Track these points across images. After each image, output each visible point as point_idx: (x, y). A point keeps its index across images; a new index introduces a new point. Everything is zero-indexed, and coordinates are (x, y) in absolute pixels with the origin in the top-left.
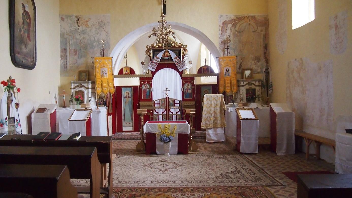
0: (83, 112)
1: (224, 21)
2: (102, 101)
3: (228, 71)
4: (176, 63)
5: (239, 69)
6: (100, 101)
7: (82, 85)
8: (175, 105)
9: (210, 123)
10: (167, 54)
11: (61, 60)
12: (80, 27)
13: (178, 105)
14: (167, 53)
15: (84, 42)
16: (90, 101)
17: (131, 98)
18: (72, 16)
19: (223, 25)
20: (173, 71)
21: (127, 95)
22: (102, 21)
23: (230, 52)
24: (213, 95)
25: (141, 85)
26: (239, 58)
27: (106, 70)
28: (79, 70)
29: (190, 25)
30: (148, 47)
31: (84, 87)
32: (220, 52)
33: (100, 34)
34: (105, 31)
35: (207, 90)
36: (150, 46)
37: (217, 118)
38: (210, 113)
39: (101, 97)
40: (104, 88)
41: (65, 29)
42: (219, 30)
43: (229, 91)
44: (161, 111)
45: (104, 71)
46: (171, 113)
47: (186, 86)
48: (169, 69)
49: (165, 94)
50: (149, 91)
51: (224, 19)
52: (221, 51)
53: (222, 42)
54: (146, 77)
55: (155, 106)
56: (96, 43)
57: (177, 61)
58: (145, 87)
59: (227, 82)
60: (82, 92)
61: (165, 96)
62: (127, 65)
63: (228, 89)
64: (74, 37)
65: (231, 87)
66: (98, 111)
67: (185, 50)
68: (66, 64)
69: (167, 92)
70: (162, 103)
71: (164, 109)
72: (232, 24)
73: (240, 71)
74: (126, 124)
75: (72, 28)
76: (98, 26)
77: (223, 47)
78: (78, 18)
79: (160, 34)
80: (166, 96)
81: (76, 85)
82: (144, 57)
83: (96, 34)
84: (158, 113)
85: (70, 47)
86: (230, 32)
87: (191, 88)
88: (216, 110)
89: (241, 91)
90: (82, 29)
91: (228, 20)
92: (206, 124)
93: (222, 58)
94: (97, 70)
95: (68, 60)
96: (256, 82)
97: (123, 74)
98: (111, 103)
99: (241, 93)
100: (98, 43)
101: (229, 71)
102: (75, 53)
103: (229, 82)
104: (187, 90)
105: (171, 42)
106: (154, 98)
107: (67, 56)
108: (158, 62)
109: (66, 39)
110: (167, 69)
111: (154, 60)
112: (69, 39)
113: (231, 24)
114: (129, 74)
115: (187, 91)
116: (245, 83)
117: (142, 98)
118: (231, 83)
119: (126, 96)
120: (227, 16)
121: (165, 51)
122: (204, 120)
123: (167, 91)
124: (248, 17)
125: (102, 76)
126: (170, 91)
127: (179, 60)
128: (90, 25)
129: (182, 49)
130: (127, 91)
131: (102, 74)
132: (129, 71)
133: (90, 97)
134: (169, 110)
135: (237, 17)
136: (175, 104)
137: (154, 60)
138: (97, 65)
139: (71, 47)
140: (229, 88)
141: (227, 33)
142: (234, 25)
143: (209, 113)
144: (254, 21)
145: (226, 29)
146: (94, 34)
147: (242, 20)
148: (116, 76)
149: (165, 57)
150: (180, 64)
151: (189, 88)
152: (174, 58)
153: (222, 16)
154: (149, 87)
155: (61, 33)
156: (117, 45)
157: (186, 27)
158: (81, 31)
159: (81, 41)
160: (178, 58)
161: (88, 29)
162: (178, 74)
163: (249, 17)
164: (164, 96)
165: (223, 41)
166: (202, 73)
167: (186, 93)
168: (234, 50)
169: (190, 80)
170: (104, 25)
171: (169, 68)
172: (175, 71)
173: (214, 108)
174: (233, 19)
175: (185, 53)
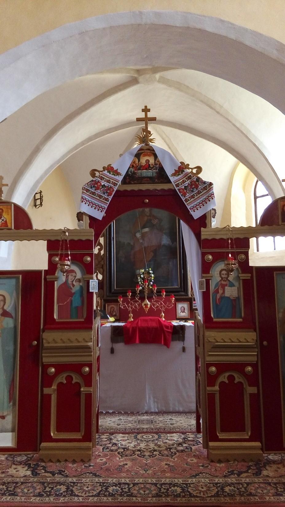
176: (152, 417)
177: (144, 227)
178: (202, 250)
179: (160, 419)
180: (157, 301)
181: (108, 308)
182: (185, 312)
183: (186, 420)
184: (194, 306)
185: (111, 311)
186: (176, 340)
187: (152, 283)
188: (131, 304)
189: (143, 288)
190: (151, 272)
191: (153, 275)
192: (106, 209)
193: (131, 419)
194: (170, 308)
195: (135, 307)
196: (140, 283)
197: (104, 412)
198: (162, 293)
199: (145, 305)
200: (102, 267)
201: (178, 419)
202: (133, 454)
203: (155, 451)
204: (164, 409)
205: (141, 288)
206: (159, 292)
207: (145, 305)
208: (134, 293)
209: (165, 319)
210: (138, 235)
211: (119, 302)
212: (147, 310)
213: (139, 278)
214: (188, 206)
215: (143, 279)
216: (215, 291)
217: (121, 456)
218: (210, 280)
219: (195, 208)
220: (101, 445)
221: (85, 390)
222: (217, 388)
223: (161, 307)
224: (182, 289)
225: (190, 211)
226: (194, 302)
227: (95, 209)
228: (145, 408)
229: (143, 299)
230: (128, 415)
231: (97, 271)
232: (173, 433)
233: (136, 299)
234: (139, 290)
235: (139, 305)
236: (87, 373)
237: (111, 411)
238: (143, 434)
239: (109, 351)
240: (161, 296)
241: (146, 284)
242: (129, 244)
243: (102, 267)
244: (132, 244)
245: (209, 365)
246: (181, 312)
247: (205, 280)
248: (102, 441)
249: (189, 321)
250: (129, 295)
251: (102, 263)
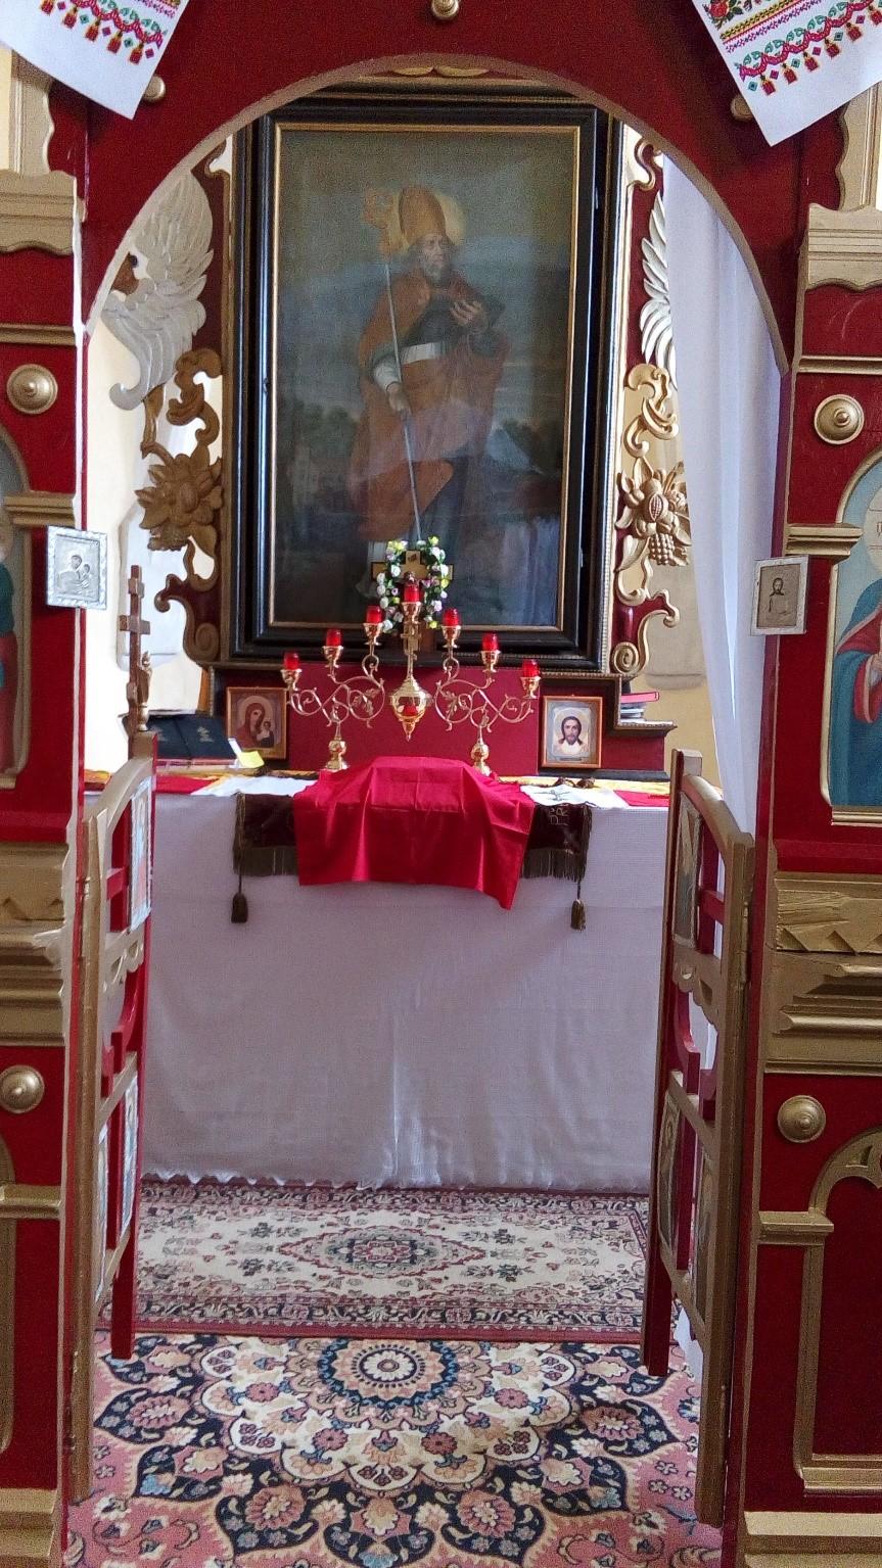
176: (415, 1216)
177: (415, 337)
178: (803, 362)
179: (453, 1233)
180: (456, 689)
181: (239, 706)
182: (580, 743)
183: (573, 1245)
184: (624, 717)
185: (248, 723)
186: (544, 874)
187: (438, 605)
188: (342, 696)
189: (399, 627)
190: (437, 552)
191: (445, 570)
192: (166, 39)
193: (311, 1228)
194: (518, 720)
195: (360, 710)
196: (385, 602)
197: (195, 1180)
198: (483, 653)
199: (405, 701)
200: (215, 523)
201: (535, 1237)
202: (296, 1525)
203: (425, 1492)
204: (471, 1175)
205: (389, 624)
206: (471, 646)
207: (405, 701)
208: (356, 647)
209: (491, 768)
210: (386, 376)
211: (285, 685)
212: (413, 726)
213: (381, 577)
214: (731, 49)
215: (402, 585)
216: (852, 640)
217: (233, 1536)
218: (835, 567)
219: (769, 68)
220: (135, 1438)
221: (18, 1201)
222: (815, 1218)
223: (478, 717)
224: (572, 637)
225: (743, 85)
226: (622, 699)
227: (92, 35)
228: (386, 1167)
229: (393, 675)
230: (304, 1200)
231: (191, 538)
232: (518, 1341)
233: (365, 675)
234: (378, 633)
235: (376, 701)
236: (33, 1101)
237: (225, 1177)
238: (366, 1344)
239: (225, 911)
240: (479, 663)
241: (411, 609)
242: (342, 415)
243: (215, 523)
244: (355, 416)
245: (783, 1087)
246: (562, 741)
247: (804, 562)
248: (149, 1394)
249: (597, 782)
250: (333, 652)
251: (214, 500)
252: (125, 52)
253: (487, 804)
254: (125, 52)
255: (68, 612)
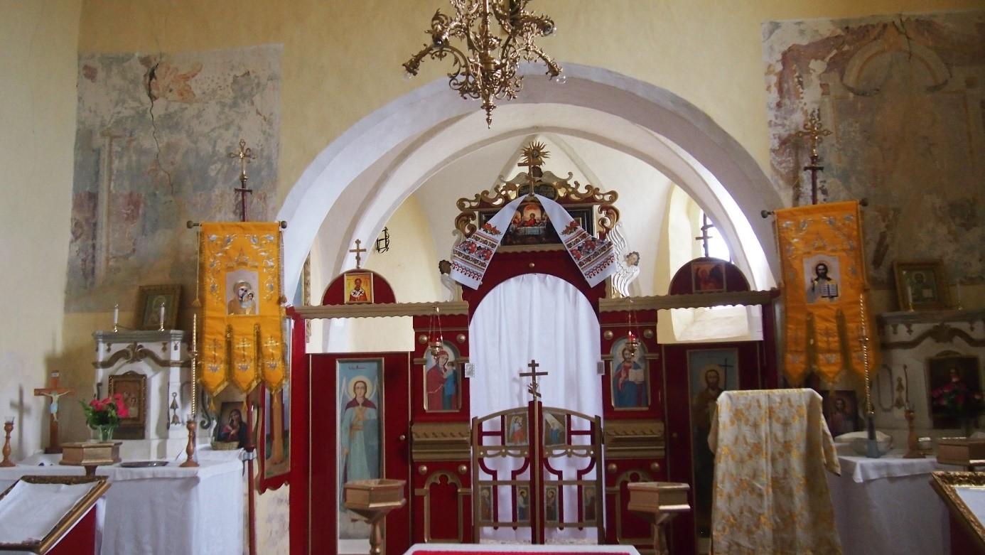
0: (58, 491)
1: (786, 48)
2: (235, 423)
3: (822, 273)
4: (571, 251)
5: (877, 262)
6: (226, 421)
7: (141, 346)
8: (573, 437)
9: (754, 543)
10: (532, 211)
11: (72, 242)
12: (160, 103)
13: (587, 440)
14: (530, 208)
15: (172, 163)
16: (173, 422)
17: (376, 404)
18: (128, 58)
19: (784, 64)
20: (561, 288)
21: (360, 392)
22: (248, 73)
23: (826, 186)
24: (767, 391)
25: (421, 348)
26: (870, 212)
27: (255, 279)
28: (144, 283)
29: (628, 73)
30: (465, 202)
31: (148, 359)
32: (776, 188)
33: (240, 128)
34: (258, 113)
35: (717, 368)
36: (474, 201)
37: (792, 515)
38: (753, 490)
39: (227, 406)
40: (238, 365)
41: (95, 112)
42: (768, 88)
43: (837, 374)
44: (507, 465)
45: (242, 284)
46: (554, 477)
47: (619, 349)
48: (546, 277)
49: (525, 392)
50: (455, 372)
51: (790, 38)
52: (781, 182)
53: (784, 142)
54: (442, 316)
55: (480, 442)
56: (219, 165)
57: (577, 241)
58: (439, 357)
59: (820, 325)
60: (139, 382)
61: (526, 398)
62: (361, 262)
63: (828, 363)
64: (130, 142)
65: (845, 350)
66: (188, 476)
67: (613, 213)
68: (90, 257)
69: (534, 379)
70: (514, 432)
71: (523, 460)
72: (827, 59)
73: (883, 273)
74: (352, 524)
75: (126, 105)
76: (232, 94)
77: (792, 165)
78: (152, 66)
79: (469, 41)
80: (532, 399)
81: (117, 347)
82: (448, 240)
83: (220, 127)
84: (494, 473)
85: (112, 188)
86: (820, 96)
87: (643, 359)
88: (786, 471)
89: (898, 372)
90: (166, 109)
91: (805, 42)
92: (735, 548)
93: (791, 215)
94: (210, 280)
95: (102, 240)
96: (971, 321)
97: (341, 301)
98: (285, 434)
99: (900, 380)
100: (226, 167)
101: (829, 275)
102: (132, 211)
103: (833, 326)
104: (627, 369)
105: (555, 183)
106: (478, 409)
107: (99, 226)
108: (493, 246)
109: (99, 154)
110: (536, 278)
111: (477, 239)
112: (110, 152)
113: (823, 59)
114: (368, 298)
115: (623, 375)
116: (918, 329)
117: (425, 407)
118: (842, 332)
119: (355, 399)
120: (802, 27)
121: (524, 201)
122: (720, 527)
123: (534, 374)
124: (898, 22)
125: (234, 307)
126: (546, 374)
127: (584, 236)
128: (198, 92)
129: (596, 208)
130: (712, 367)
131: (230, 297)
132: (368, 289)
133: (174, 406)
134: (544, 461)
135: (847, 28)
136: (571, 433)
137: (477, 239)
138: (214, 260)
139: (114, 187)
140: (835, 358)
141: (803, 101)
142: (839, 65)
143: (747, 487)
144: (930, 43)
145: (800, 83)
146: (213, 130)
147: (875, 39)
148: (316, 313)
149: (524, 224)
150: (592, 252)
151: (636, 359)
152: (565, 228)
153: (776, 26)
154: (456, 355)
155: (78, 131)
156: (307, 173)
157: (612, 83)
158: (160, 116)
159: (157, 162)
160: (580, 228)
161: (192, 110)
162: (582, 298)
163: (903, 25)
164: (520, 396)
165: (790, 136)
166: (690, 292)
167: (621, 380)
168: (845, 177)
169: (637, 325)
170: (255, 91)
171: (542, 275)
172: (571, 286)
173: (774, 460)
174: (828, 38)
175: (608, 223)
219: (591, 273)
225: (585, 277)
252: (475, 279)
253: (480, 497)
254: (475, 279)
255: (469, 378)
